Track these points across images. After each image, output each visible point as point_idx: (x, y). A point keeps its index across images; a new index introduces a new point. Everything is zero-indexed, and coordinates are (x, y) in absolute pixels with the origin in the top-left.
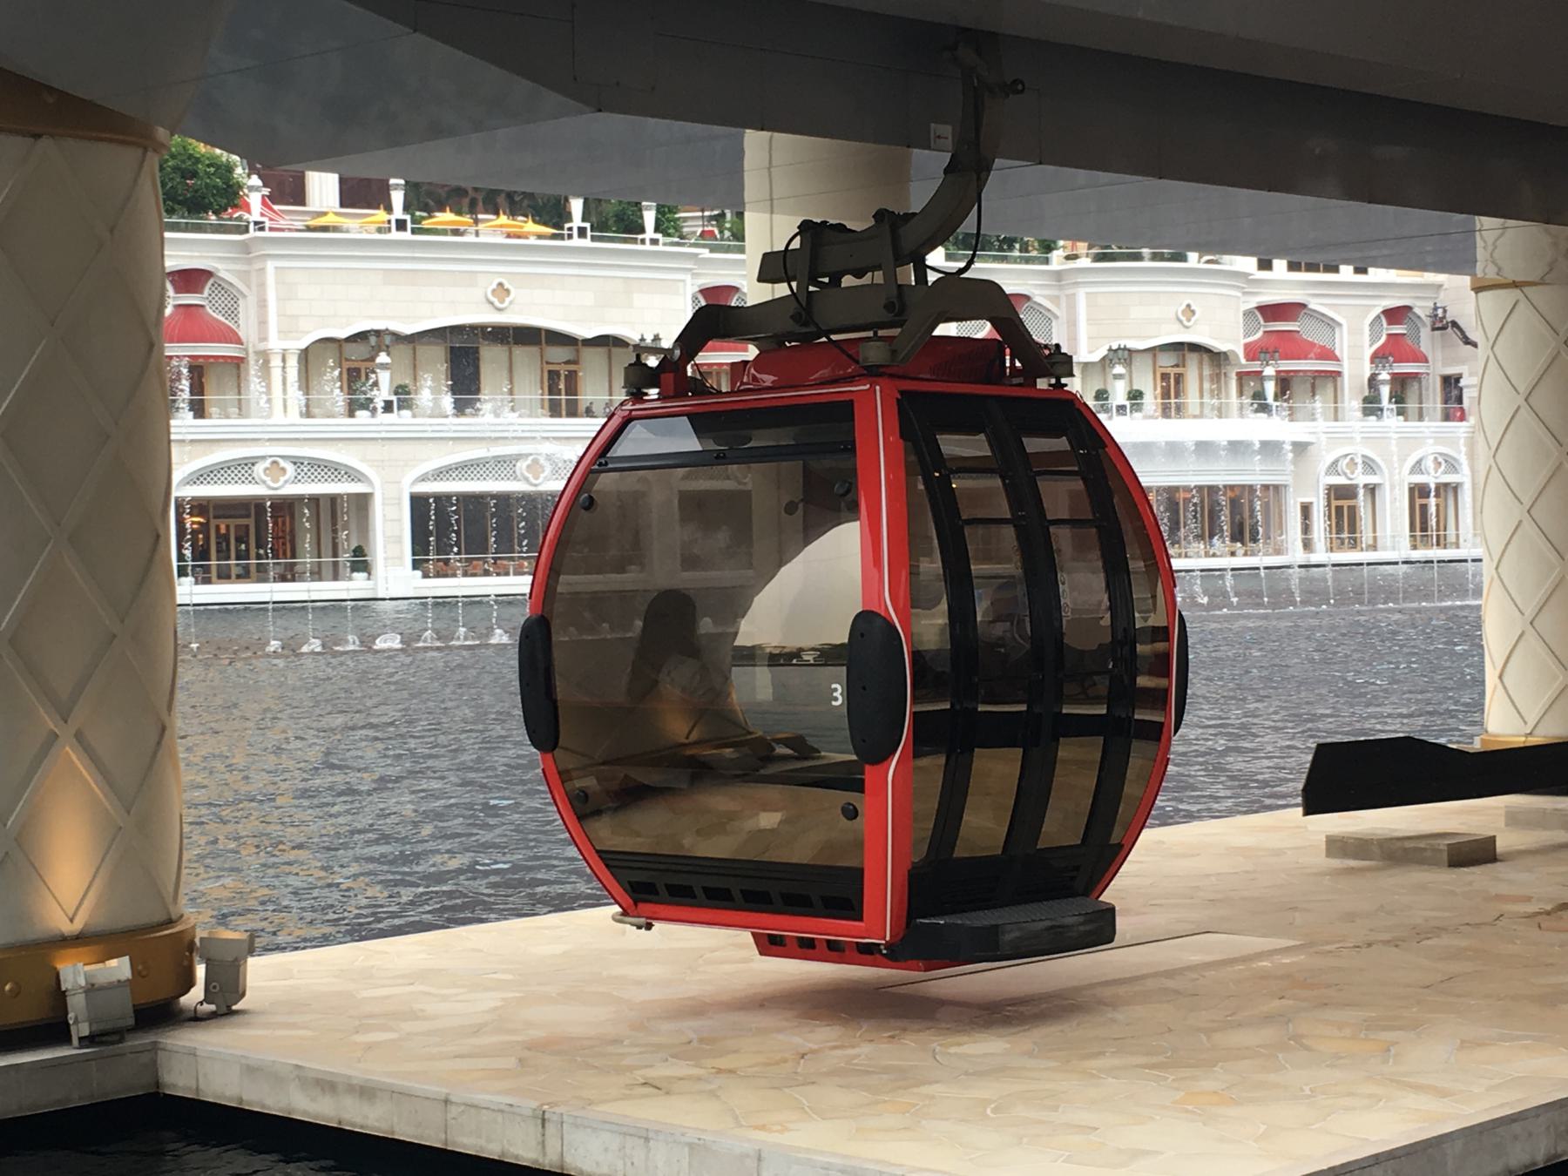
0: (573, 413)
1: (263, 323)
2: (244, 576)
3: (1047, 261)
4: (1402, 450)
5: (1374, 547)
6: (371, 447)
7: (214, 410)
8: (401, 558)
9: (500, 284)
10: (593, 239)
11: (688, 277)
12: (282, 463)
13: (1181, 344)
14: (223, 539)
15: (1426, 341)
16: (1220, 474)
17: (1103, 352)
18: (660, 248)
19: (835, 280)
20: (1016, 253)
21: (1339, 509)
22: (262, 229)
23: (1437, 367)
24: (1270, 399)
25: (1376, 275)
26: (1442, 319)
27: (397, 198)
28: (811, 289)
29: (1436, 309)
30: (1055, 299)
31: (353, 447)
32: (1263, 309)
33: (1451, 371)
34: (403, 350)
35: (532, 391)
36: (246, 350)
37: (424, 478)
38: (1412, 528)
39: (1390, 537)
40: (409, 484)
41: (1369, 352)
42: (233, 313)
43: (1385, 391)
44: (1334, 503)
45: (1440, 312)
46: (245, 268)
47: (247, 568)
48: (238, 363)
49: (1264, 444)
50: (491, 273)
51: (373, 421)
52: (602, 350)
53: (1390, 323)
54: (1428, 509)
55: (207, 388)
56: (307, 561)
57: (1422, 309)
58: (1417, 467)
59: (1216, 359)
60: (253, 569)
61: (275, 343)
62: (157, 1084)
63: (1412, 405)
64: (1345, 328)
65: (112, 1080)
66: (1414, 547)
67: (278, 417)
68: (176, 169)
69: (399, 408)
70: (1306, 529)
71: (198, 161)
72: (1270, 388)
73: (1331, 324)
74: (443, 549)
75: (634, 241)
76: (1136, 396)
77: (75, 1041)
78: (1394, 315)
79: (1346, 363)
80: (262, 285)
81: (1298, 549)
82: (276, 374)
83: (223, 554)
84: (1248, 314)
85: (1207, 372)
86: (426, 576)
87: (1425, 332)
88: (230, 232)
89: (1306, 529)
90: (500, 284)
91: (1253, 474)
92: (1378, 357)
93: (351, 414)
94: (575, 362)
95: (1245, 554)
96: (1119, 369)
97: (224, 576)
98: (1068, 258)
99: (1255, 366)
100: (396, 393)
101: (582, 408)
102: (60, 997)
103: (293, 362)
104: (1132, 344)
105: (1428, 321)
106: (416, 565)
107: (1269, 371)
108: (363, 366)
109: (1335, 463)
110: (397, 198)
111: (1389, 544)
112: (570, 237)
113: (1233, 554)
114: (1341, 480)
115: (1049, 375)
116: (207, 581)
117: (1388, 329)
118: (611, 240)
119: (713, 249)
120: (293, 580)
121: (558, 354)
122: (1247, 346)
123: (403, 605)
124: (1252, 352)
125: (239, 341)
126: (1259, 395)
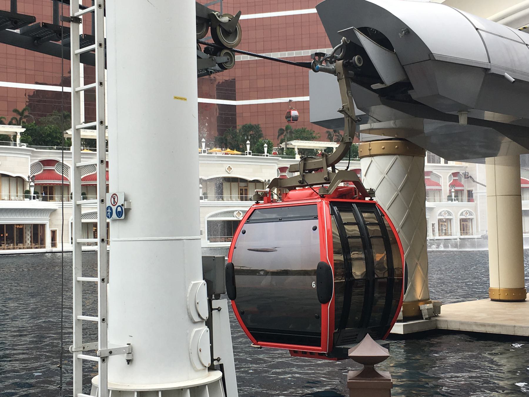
0: (246, 200)
5: (451, 235)
11: (276, 165)
13: (211, 179)
15: (463, 181)
18: (268, 157)
20: (358, 158)
23: (466, 188)
24: (453, 197)
25: (451, 163)
35: (236, 194)
38: (461, 230)
39: (456, 233)
41: (448, 184)
43: (453, 194)
44: (462, 223)
50: (227, 164)
52: (254, 184)
59: (19, 180)
63: (460, 198)
65: (431, 327)
70: (433, 231)
73: (438, 177)
75: (262, 156)
78: (455, 174)
86: (210, 242)
89: (433, 231)
94: (247, 187)
101: (249, 198)
102: (420, 311)
106: (208, 239)
109: (441, 213)
114: (464, 217)
117: (453, 178)
119: (282, 158)
121: (243, 184)
125: (440, 186)
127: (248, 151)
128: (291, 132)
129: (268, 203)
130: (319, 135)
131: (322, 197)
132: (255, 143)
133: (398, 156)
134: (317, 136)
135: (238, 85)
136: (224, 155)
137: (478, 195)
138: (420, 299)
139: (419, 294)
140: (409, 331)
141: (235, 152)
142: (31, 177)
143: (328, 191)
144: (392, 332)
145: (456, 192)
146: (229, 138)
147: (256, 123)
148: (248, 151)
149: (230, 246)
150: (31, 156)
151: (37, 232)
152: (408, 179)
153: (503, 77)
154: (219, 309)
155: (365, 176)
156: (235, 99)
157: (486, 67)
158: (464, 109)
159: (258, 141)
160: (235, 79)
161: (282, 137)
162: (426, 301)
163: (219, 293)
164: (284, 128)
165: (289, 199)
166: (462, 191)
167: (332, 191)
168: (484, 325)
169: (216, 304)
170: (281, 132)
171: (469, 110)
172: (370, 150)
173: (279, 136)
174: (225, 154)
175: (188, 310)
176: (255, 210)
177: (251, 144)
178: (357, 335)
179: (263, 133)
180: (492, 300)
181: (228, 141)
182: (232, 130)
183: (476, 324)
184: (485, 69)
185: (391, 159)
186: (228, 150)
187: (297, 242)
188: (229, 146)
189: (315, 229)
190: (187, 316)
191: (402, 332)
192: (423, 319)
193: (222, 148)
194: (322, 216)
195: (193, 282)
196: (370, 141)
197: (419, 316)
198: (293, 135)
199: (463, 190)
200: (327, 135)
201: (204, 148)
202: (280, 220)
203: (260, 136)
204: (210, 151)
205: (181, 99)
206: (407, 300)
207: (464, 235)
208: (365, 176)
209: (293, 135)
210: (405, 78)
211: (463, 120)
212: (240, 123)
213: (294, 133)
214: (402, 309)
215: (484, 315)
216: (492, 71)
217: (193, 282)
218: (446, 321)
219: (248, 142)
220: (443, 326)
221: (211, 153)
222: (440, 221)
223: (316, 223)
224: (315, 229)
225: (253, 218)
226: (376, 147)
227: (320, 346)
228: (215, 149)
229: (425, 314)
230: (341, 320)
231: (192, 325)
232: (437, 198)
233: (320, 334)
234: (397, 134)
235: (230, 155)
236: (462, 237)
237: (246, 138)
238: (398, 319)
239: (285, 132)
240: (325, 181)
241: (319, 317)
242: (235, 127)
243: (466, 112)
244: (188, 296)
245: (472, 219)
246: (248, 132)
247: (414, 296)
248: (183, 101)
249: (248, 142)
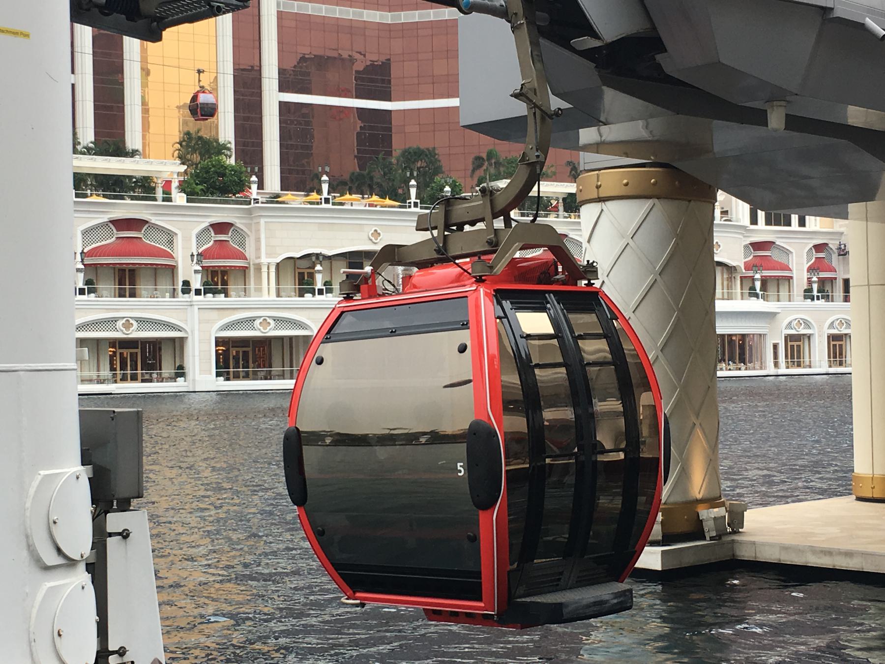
1: (258, 249)
2: (247, 377)
4: (822, 318)
5: (810, 367)
6: (312, 312)
8: (210, 371)
9: (376, 231)
10: (421, 208)
12: (269, 320)
14: (236, 359)
15: (835, 261)
19: (460, 227)
22: (258, 203)
23: (840, 276)
24: (815, 293)
26: (843, 250)
27: (325, 187)
28: (446, 233)
29: (840, 245)
30: (249, 226)
31: (307, 312)
32: (113, 222)
33: (846, 277)
34: (326, 263)
35: (113, 287)
36: (249, 264)
37: (227, 327)
38: (829, 357)
39: (818, 360)
40: (215, 332)
41: (806, 266)
42: (242, 244)
43: (815, 287)
44: (832, 343)
45: (842, 246)
46: (250, 222)
48: (244, 270)
51: (313, 299)
53: (816, 252)
54: (837, 346)
55: (138, 282)
56: (276, 369)
57: (833, 245)
60: (251, 374)
61: (264, 260)
62: (733, 555)
66: (830, 366)
67: (265, 297)
68: (215, 172)
69: (205, 294)
70: (776, 356)
71: (226, 168)
72: (758, 285)
73: (787, 252)
77: (708, 538)
78: (819, 248)
79: (794, 272)
81: (770, 366)
83: (237, 366)
84: (746, 247)
85: (725, 276)
87: (835, 257)
89: (776, 356)
90: (376, 231)
92: (811, 269)
93: (301, 295)
95: (746, 369)
97: (237, 377)
99: (750, 273)
100: (325, 285)
103: (273, 269)
105: (836, 251)
107: (758, 276)
108: (306, 271)
109: (790, 323)
110: (325, 187)
111: (817, 364)
112: (410, 207)
113: (740, 369)
115: (584, 278)
116: (228, 379)
118: (215, 202)
120: (271, 379)
122: (745, 263)
123: (207, 396)
124: (748, 267)
126: (753, 288)
127: (413, 199)
128: (498, 164)
129: (370, 297)
130: (553, 169)
131: (480, 280)
132: (427, 185)
133: (656, 201)
134: (549, 171)
135: (395, 72)
136: (367, 208)
138: (699, 496)
139: (698, 487)
140: (674, 565)
141: (388, 202)
143: (491, 268)
144: (638, 565)
145: (822, 282)
146: (378, 175)
147: (431, 146)
148: (413, 199)
149: (292, 387)
152: (676, 244)
153: (862, 26)
154: (125, 535)
155: (589, 241)
156: (388, 98)
157: (824, 5)
158: (778, 95)
159: (432, 180)
160: (389, 60)
161: (480, 173)
162: (712, 501)
163: (126, 495)
164: (484, 156)
165: (415, 287)
166: (832, 280)
167: (500, 268)
168: (829, 553)
169: (115, 521)
170: (478, 162)
171: (788, 98)
172: (598, 187)
173: (473, 171)
174: (370, 205)
175: (27, 537)
176: (342, 313)
177: (418, 187)
178: (561, 573)
179: (444, 163)
180: (859, 499)
181: (375, 180)
182: (384, 159)
183: (814, 550)
184: (822, 8)
185: (640, 208)
186: (375, 198)
187: (424, 380)
188: (377, 190)
189: (462, 349)
190: (25, 553)
191: (658, 566)
192: (704, 538)
193: (362, 194)
194: (479, 322)
195: (43, 473)
196: (600, 170)
197: (697, 533)
198: (502, 169)
199: (835, 278)
200: (569, 169)
201: (325, 194)
202: (393, 333)
203: (438, 170)
204: (337, 200)
205: (15, 33)
206: (672, 500)
207: (836, 366)
208: (589, 241)
209: (502, 169)
210: (648, 26)
211: (776, 120)
212: (398, 145)
213: (503, 166)
214: (660, 517)
215: (834, 531)
216: (838, 13)
217: (43, 473)
218: (754, 543)
219: (413, 182)
220: (746, 554)
221: (341, 204)
223: (464, 336)
224: (462, 349)
225: (337, 330)
226: (611, 181)
227: (480, 600)
228: (348, 196)
229: (710, 529)
230: (525, 540)
231: (39, 575)
232: (784, 293)
233: (478, 575)
234: (656, 156)
235: (378, 208)
236: (832, 370)
237: (408, 174)
238: (650, 538)
239: (486, 163)
240: (487, 248)
241: (474, 539)
242: (389, 153)
243: (783, 103)
244: (28, 505)
245: (809, 337)
246: (414, 163)
247: (686, 491)
248: (20, 39)
249: (413, 182)
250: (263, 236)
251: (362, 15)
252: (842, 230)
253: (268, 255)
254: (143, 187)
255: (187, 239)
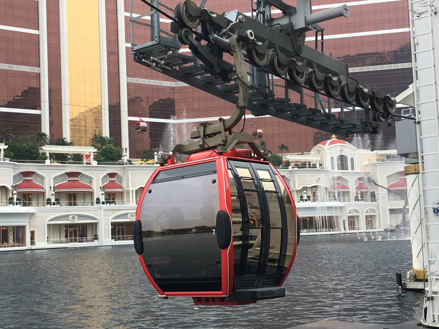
1: (128, 184)
2: (123, 239)
3: (288, 169)
7: (117, 203)
8: (109, 237)
12: (75, 216)
16: (327, 214)
17: (301, 187)
20: (281, 167)
21: (351, 221)
23: (370, 190)
30: (290, 177)
32: (67, 174)
38: (349, 226)
42: (121, 182)
43: (359, 195)
47: (123, 237)
48: (122, 193)
49: (340, 207)
58: (367, 212)
60: (125, 238)
61: (131, 188)
64: (46, 179)
66: (349, 230)
67: (131, 204)
73: (42, 178)
74: (75, 236)
76: (309, 197)
78: (360, 179)
80: (128, 176)
81: (342, 229)
82: (131, 195)
88: (35, 163)
91: (333, 213)
96: (305, 191)
98: (293, 168)
103: (134, 193)
104: (307, 186)
106: (112, 238)
109: (350, 211)
114: (368, 214)
119: (299, 168)
124: (14, 187)
137: (380, 195)
142: (102, 186)
145: (362, 193)
150: (13, 169)
151: (19, 231)
222: (349, 217)
245: (358, 217)
250: (130, 178)
251: (162, 83)
252: (369, 171)
253: (132, 186)
254: (78, 158)
255: (49, 180)
